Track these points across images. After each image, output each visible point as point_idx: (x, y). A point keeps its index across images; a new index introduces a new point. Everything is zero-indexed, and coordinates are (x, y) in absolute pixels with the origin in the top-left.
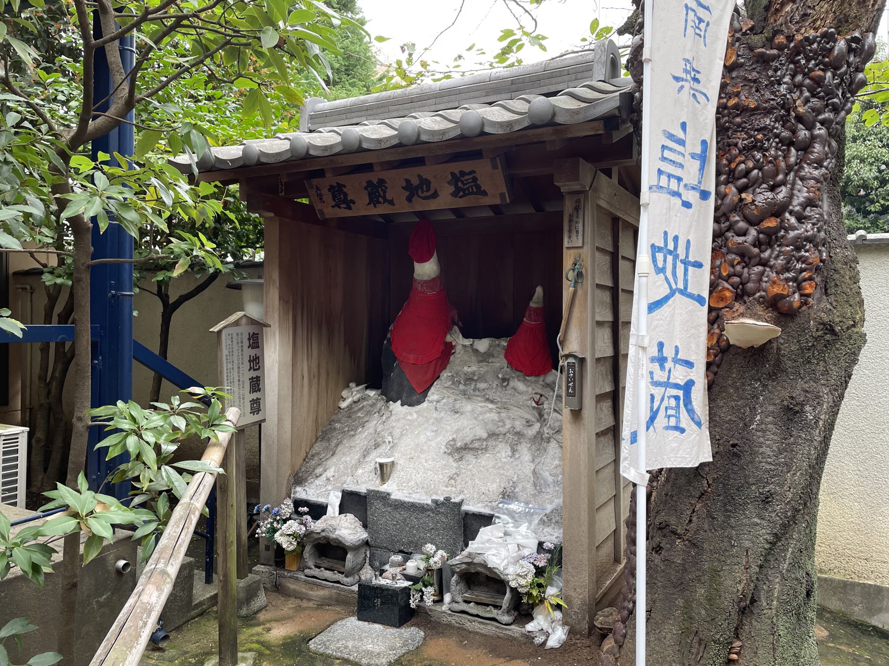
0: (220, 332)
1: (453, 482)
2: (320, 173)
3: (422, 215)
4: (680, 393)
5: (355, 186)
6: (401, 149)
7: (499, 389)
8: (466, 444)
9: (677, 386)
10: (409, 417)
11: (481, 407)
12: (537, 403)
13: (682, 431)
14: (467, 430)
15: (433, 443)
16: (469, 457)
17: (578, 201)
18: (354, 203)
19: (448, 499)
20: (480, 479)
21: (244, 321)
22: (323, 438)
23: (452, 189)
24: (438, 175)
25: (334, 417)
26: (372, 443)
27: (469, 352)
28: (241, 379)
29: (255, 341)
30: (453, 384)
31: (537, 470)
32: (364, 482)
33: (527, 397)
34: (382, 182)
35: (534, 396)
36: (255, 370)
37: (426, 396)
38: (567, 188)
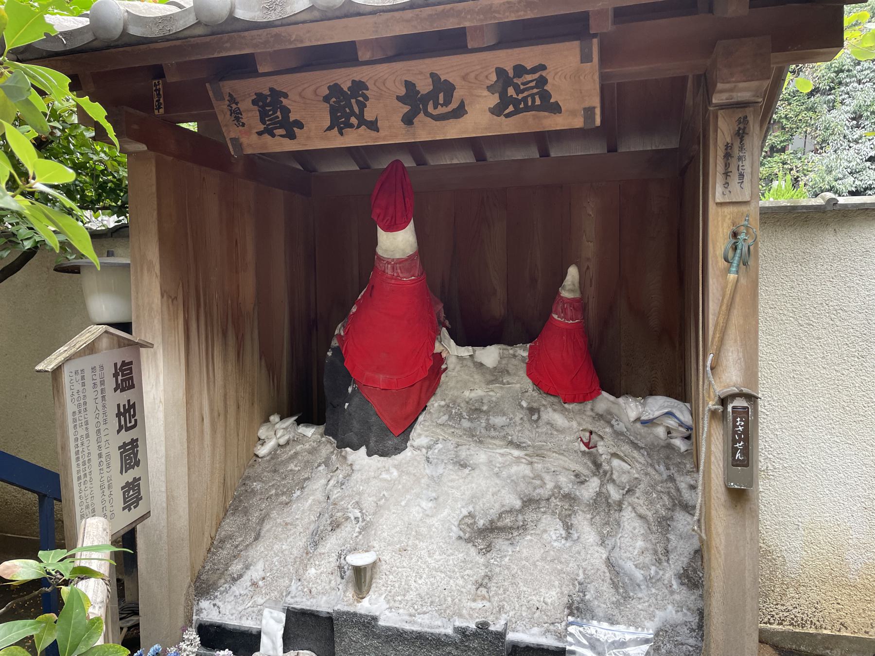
0: (58, 369)
1: (483, 591)
2: (243, 66)
5: (306, 96)
7: (527, 425)
8: (492, 522)
10: (384, 476)
11: (502, 455)
12: (587, 445)
14: (489, 496)
15: (434, 521)
16: (500, 543)
17: (744, 120)
18: (300, 125)
19: (483, 626)
20: (526, 582)
21: (105, 342)
22: (236, 510)
23: (494, 100)
25: (249, 472)
26: (326, 520)
27: (471, 370)
28: (104, 452)
29: (127, 377)
30: (451, 417)
31: (613, 560)
32: (328, 597)
33: (572, 437)
34: (359, 87)
35: (582, 434)
36: (128, 429)
37: (408, 439)
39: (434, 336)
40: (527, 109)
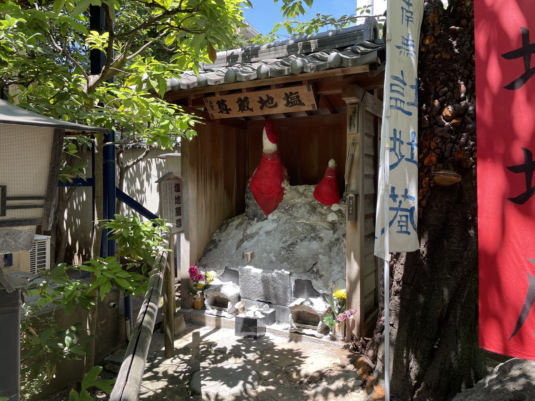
2: (213, 94)
3: (266, 116)
4: (408, 214)
5: (231, 101)
6: (257, 81)
9: (406, 210)
13: (409, 233)
18: (230, 110)
23: (285, 102)
24: (278, 95)
34: (246, 98)
38: (349, 101)
39: (282, 181)
40: (295, 105)
